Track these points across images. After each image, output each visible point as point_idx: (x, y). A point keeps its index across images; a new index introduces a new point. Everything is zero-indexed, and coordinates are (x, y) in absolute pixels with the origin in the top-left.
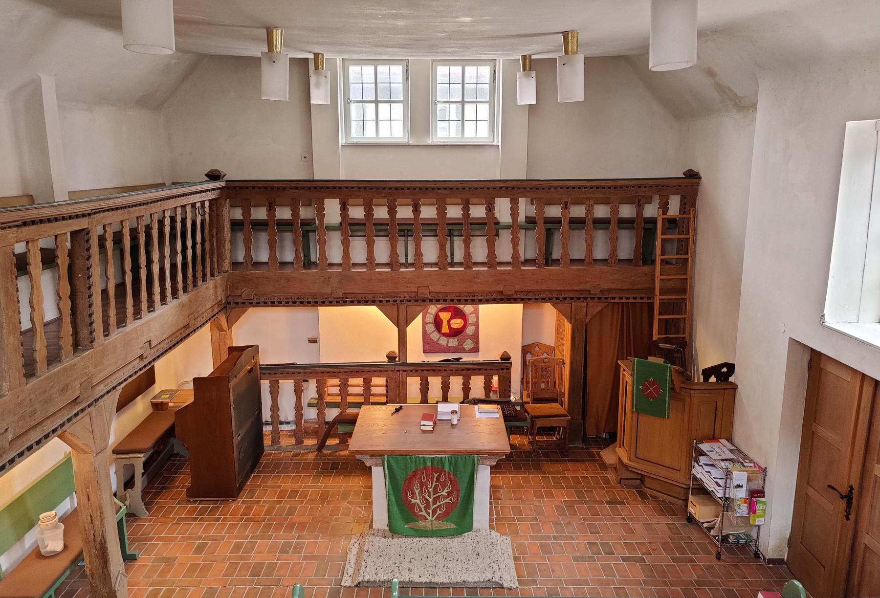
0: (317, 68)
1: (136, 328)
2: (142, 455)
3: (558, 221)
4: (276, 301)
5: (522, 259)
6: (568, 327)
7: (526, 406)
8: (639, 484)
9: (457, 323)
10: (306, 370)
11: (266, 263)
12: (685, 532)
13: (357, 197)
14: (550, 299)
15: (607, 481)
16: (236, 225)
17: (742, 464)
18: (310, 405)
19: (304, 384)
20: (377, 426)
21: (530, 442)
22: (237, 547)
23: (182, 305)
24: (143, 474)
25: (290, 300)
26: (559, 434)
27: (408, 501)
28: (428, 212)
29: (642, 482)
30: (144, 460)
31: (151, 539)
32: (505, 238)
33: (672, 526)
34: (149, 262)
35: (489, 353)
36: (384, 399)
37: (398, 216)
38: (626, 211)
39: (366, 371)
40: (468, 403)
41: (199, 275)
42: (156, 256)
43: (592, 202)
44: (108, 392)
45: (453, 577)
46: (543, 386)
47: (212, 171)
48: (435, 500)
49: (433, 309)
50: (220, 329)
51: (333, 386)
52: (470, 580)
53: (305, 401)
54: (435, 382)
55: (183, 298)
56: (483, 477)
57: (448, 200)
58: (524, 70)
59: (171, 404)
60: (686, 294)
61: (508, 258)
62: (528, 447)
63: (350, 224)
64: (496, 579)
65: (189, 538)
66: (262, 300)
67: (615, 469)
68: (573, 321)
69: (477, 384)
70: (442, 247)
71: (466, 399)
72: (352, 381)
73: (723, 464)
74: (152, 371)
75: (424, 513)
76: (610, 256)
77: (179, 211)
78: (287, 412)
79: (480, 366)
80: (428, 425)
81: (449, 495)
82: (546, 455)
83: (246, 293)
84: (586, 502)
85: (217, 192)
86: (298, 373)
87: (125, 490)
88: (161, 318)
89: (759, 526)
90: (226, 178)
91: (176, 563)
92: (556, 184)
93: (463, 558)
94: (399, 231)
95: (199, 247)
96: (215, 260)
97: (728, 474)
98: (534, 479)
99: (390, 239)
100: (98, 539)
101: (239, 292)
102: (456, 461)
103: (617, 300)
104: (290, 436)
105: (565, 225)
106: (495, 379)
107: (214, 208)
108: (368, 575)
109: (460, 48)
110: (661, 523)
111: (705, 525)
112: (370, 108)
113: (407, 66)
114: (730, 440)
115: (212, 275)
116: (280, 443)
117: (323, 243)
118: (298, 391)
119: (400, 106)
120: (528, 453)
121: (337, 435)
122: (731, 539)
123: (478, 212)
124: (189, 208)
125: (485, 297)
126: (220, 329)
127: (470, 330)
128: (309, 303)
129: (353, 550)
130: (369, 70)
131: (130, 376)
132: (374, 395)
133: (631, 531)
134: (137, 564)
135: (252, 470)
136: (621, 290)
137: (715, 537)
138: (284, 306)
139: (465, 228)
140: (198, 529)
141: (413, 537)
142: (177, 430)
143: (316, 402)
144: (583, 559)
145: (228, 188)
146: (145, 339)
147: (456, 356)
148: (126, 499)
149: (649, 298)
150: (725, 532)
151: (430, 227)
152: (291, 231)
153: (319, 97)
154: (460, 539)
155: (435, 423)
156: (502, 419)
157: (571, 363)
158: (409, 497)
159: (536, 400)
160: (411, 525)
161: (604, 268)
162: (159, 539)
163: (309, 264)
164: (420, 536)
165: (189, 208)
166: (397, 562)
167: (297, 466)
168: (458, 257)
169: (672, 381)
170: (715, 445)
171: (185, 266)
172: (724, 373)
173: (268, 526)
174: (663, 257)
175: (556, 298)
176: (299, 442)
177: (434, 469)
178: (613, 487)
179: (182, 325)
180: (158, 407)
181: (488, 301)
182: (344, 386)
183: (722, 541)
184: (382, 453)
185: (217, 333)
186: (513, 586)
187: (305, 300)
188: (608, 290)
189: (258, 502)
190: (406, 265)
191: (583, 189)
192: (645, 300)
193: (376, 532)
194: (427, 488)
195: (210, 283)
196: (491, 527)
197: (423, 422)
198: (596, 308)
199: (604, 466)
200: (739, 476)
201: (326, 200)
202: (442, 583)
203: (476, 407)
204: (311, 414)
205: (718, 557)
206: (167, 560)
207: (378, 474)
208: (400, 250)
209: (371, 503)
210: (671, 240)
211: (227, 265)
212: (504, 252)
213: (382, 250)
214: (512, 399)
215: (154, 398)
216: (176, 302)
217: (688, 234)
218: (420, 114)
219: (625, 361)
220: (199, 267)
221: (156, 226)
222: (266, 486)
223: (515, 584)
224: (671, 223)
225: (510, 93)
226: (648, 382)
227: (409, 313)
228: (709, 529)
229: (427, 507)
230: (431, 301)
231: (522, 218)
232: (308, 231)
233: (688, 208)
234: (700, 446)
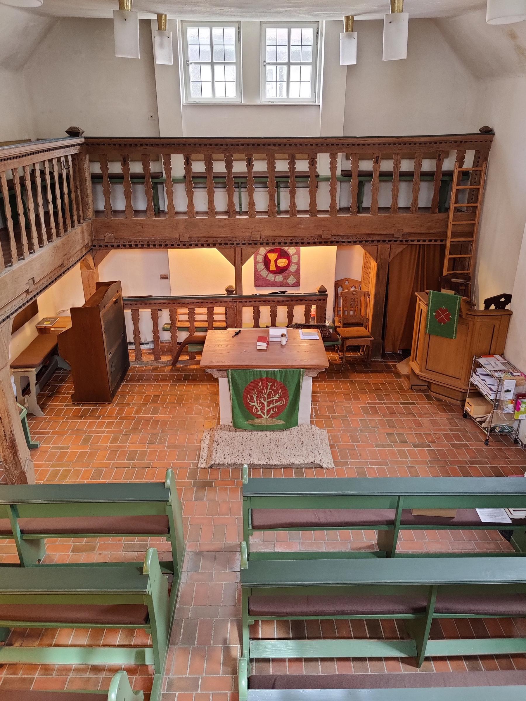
0: (160, 28)
1: (21, 266)
2: (34, 370)
3: (369, 174)
4: (133, 244)
5: (338, 208)
6: (374, 265)
7: (338, 329)
8: (426, 389)
9: (282, 262)
10: (160, 301)
11: (124, 212)
12: (461, 425)
13: (199, 152)
14: (361, 242)
15: (401, 387)
16: (96, 178)
17: (512, 374)
18: (164, 329)
19: (159, 312)
20: (219, 346)
21: (340, 358)
22: (115, 439)
23: (57, 248)
24: (36, 384)
25: (145, 243)
26: (363, 351)
27: (247, 404)
28: (260, 166)
29: (429, 387)
30: (36, 373)
31: (48, 433)
32: (324, 189)
33: (451, 421)
35: (308, 286)
36: (224, 325)
37: (234, 170)
38: (427, 165)
39: (209, 302)
40: (292, 327)
41: (69, 222)
42: (31, 205)
43: (399, 157)
44: (4, 320)
45: (284, 460)
46: (351, 313)
47: (71, 128)
48: (269, 403)
49: (262, 251)
50: (88, 267)
51: (183, 314)
52: (297, 462)
53: (160, 326)
54: (265, 311)
55: (57, 241)
56: (307, 385)
57: (277, 156)
58: (347, 30)
59: (52, 329)
60: (472, 236)
61: (244, 208)
62: (339, 361)
63: (193, 177)
64: (317, 462)
65: (77, 432)
66: (122, 243)
67: (408, 378)
68: (379, 260)
69: (299, 312)
70: (272, 197)
71: (290, 324)
72: (198, 310)
73: (496, 374)
74: (35, 302)
75: (260, 413)
76: (412, 205)
77: (47, 164)
78: (147, 335)
79: (302, 298)
80: (263, 345)
81: (280, 399)
82: (353, 367)
83: (107, 237)
84: (385, 404)
85: (78, 147)
86: (154, 303)
87: (23, 396)
88: (40, 258)
89: (520, 421)
90: (84, 135)
91: (69, 451)
92: (369, 141)
93: (291, 446)
94: (235, 183)
95: (66, 197)
96: (81, 209)
97: (500, 382)
98: (343, 386)
100: (8, 435)
101: (102, 237)
102: (286, 374)
103: (415, 243)
104: (150, 354)
105: (376, 177)
106: (314, 308)
107: (76, 163)
108: (218, 459)
109: (293, 7)
110: (443, 418)
111: (478, 420)
112: (206, 69)
113: (239, 28)
114: (502, 355)
115: (79, 222)
116: (142, 361)
117: (170, 194)
118: (155, 318)
120: (339, 366)
121: (187, 353)
122: (498, 430)
123: (302, 166)
124: (55, 162)
126: (88, 267)
128: (161, 245)
129: (206, 441)
130: (205, 32)
131: (20, 307)
132: (216, 321)
133: (420, 425)
134: (39, 451)
135: (121, 381)
136: (419, 234)
137: (485, 428)
139: (290, 180)
140: (83, 425)
141: (251, 430)
142: (60, 350)
143: (169, 327)
144: (383, 446)
145: (87, 145)
146: (29, 276)
147: (282, 289)
148: (25, 403)
149: (442, 241)
150: (493, 425)
151: (262, 180)
152: (143, 183)
153: (162, 58)
154: (288, 432)
155: (268, 344)
156: (322, 340)
157: (376, 295)
158: (249, 401)
159: (346, 325)
160: (251, 422)
161: (407, 215)
162: (54, 433)
163: (159, 213)
164: (257, 430)
165: (55, 162)
166: (241, 449)
167: (157, 378)
168: (285, 205)
169: (460, 309)
170: (490, 359)
171: (56, 213)
172: (502, 302)
173: (138, 424)
174: (456, 205)
175: (364, 241)
176: (157, 358)
177: (268, 380)
178: (406, 392)
179: (58, 265)
180: (42, 331)
181: (309, 244)
182: (192, 314)
183: (491, 431)
184: (227, 367)
185: (86, 271)
186: (330, 466)
187: (157, 243)
188: (409, 234)
189: (128, 405)
190: (240, 213)
192: (439, 242)
193: (222, 427)
194: (263, 394)
195: (78, 229)
196: (312, 423)
197: (258, 343)
198: (398, 249)
199: (398, 375)
200: (509, 383)
201: (172, 156)
202: (276, 465)
203: (300, 331)
204: (166, 336)
205: (486, 443)
206: (62, 448)
207: (224, 384)
208: (236, 200)
209: (217, 405)
210: (464, 190)
211: (90, 213)
212: (323, 201)
214: (327, 324)
215: (38, 324)
216: (51, 245)
217: (479, 185)
218: (250, 78)
219: (422, 293)
220: (68, 215)
221: (28, 178)
222: (133, 393)
223: (331, 465)
224: (465, 174)
225: (333, 53)
226: (441, 310)
227: (243, 255)
228: (481, 423)
229: (262, 409)
230: (262, 244)
231: (338, 172)
232: (156, 184)
233: (480, 162)
234: (478, 360)
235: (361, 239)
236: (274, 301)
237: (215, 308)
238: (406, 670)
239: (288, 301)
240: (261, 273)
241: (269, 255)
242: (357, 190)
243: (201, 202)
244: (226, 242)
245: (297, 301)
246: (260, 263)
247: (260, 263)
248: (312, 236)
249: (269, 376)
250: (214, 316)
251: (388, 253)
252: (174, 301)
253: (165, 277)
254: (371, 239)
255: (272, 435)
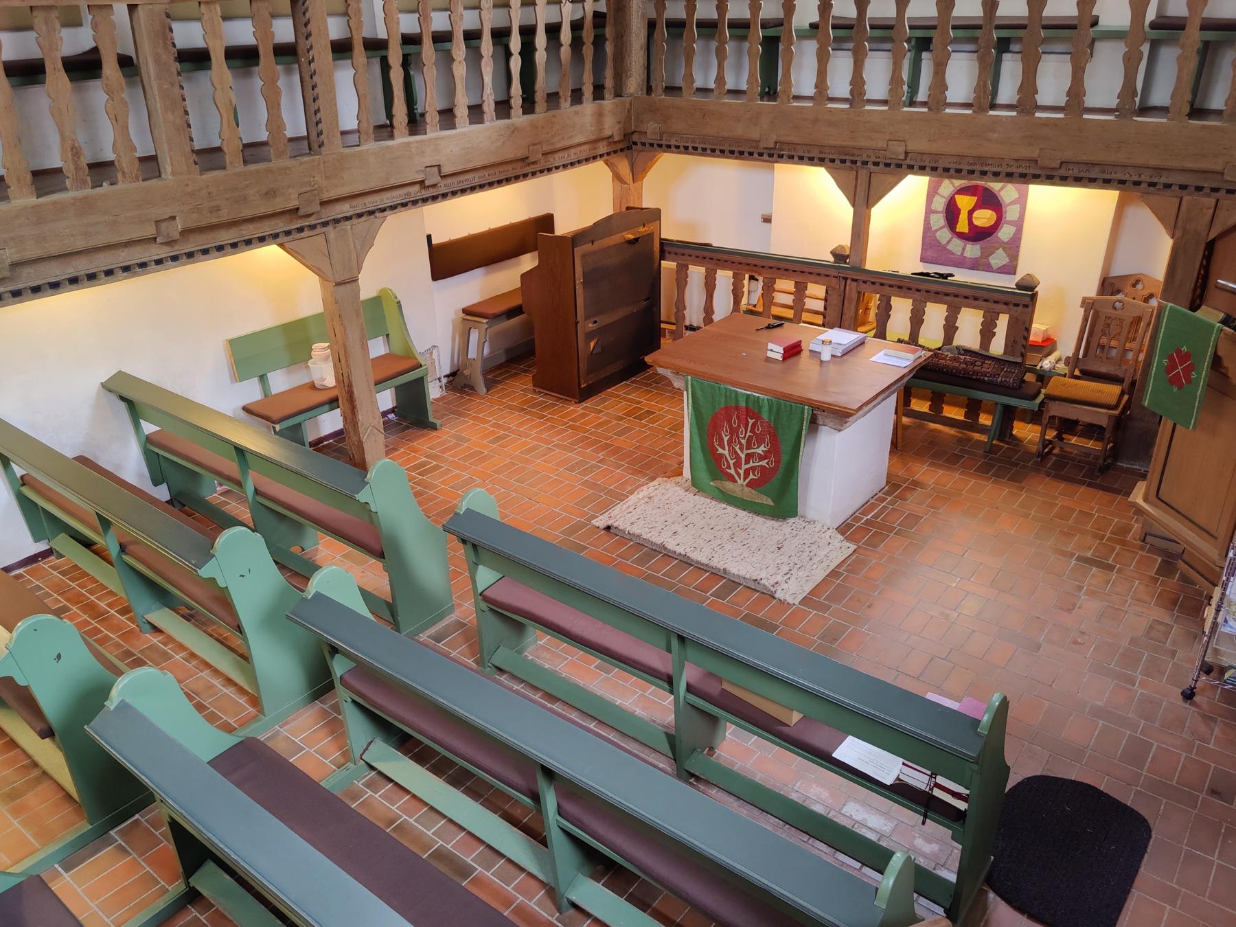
9: (984, 218)
27: (714, 450)
39: (801, 270)
68: (1178, 233)
99: (894, 57)
100: (346, 380)
106: (1003, 322)
125: (1004, 169)
127: (1005, 233)
138: (736, 158)
141: (721, 501)
158: (716, 444)
160: (718, 483)
168: (1008, 91)
177: (749, 413)
202: (698, 562)
213: (878, 73)
229: (738, 465)
235: (1135, 178)
236: (918, 290)
237: (809, 285)
238: (539, 904)
239: (947, 295)
240: (938, 234)
241: (957, 197)
242: (1193, 63)
244: (844, 157)
245: (966, 297)
246: (937, 212)
247: (937, 212)
248: (1017, 160)
249: (751, 406)
250: (806, 300)
251: (1209, 216)
252: (739, 259)
253: (767, 220)
254: (1164, 180)
255: (749, 521)
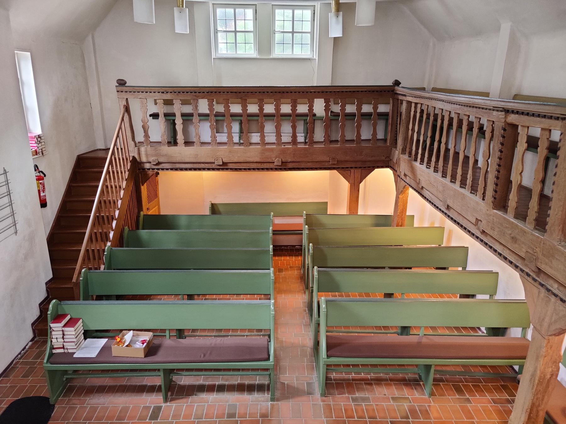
32: (269, 128)
34: (440, 142)
37: (265, 112)
105: (195, 119)
119: (252, 34)
123: (302, 109)
191: (293, 93)
225: (325, 28)
243: (366, 134)
